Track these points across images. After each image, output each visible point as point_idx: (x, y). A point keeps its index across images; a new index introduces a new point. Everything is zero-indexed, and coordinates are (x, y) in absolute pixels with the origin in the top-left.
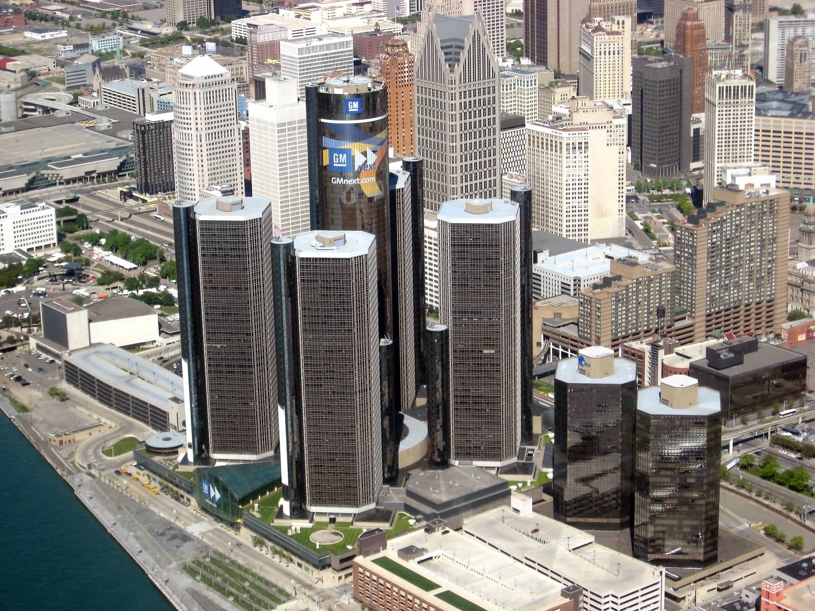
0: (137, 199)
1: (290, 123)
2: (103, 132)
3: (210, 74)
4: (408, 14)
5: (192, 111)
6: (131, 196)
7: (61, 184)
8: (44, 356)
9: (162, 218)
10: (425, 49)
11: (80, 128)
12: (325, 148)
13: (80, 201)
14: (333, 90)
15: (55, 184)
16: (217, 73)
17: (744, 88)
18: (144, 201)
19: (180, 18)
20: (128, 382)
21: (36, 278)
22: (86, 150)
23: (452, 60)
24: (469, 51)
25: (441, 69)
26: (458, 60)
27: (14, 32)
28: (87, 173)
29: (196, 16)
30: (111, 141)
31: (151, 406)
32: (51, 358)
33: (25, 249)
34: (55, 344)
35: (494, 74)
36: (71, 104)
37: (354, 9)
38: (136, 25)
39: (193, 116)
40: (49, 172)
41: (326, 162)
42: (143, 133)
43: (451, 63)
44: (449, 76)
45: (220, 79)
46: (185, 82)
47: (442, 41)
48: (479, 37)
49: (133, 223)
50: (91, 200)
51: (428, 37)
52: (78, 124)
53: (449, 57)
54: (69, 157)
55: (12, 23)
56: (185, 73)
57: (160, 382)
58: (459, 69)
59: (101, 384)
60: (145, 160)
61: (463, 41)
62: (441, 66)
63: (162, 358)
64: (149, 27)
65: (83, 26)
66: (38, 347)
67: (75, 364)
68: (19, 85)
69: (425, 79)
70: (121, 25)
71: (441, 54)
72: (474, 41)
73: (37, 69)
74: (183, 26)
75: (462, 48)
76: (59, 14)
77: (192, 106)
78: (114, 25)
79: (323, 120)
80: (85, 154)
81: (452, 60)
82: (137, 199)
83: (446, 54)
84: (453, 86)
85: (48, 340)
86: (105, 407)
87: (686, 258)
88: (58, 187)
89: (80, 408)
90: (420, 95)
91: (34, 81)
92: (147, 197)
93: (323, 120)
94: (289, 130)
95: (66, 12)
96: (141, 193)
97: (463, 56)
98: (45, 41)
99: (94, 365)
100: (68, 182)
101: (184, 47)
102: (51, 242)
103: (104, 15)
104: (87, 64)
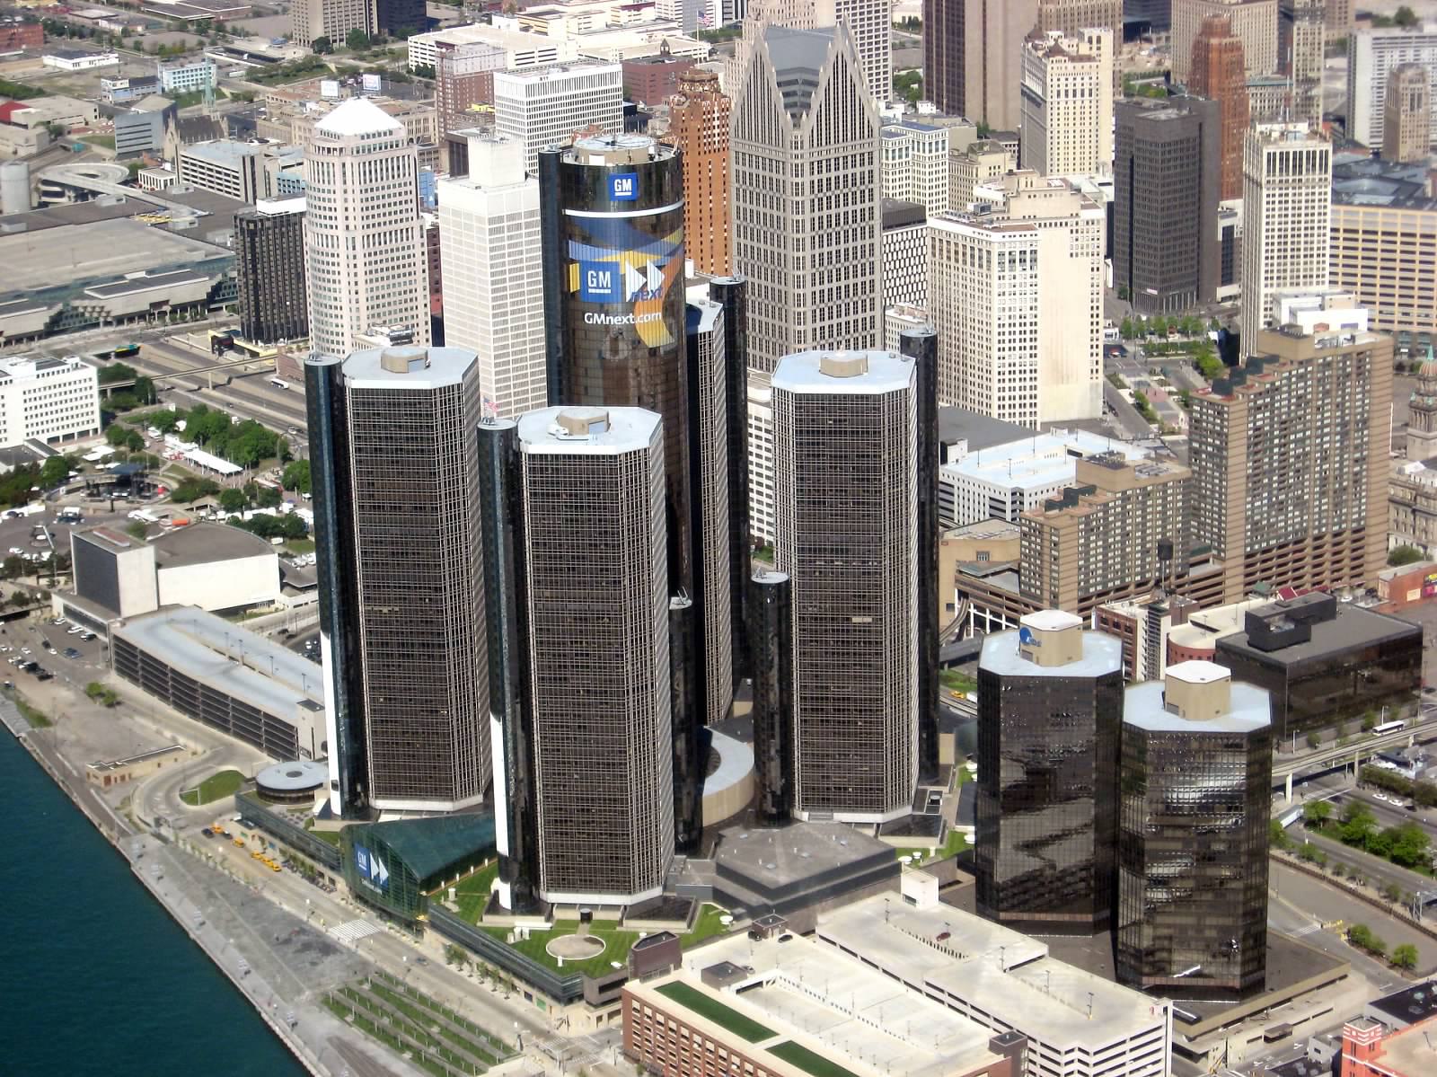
0: (241, 350)
1: (511, 217)
2: (182, 233)
3: (371, 131)
4: (719, 24)
5: (339, 196)
6: (231, 346)
7: (107, 324)
8: (77, 627)
9: (286, 385)
10: (749, 86)
11: (141, 226)
12: (573, 261)
13: (141, 354)
14: (587, 159)
15: (96, 325)
16: (382, 129)
17: (1311, 156)
18: (254, 355)
19: (318, 31)
20: (226, 673)
21: (63, 489)
22: (152, 264)
23: (798, 106)
24: (827, 90)
25: (777, 121)
26: (808, 106)
27: (25, 56)
28: (154, 305)
29: (346, 29)
30: (195, 249)
31: (267, 715)
32: (90, 632)
33: (43, 439)
34: (97, 606)
35: (871, 131)
36: (125, 183)
37: (624, 16)
38: (239, 44)
39: (339, 205)
40: (86, 303)
41: (575, 286)
42: (253, 234)
43: (795, 110)
44: (792, 134)
45: (388, 139)
46: (327, 145)
47: (779, 73)
48: (845, 66)
49: (234, 393)
50: (160, 352)
51: (755, 66)
52: (137, 218)
53: (791, 100)
54: (122, 277)
55: (22, 41)
56: (326, 128)
57: (282, 673)
58: (809, 121)
59: (179, 677)
60: (255, 282)
61: (816, 73)
62: (777, 116)
63: (285, 631)
64: (262, 47)
65: (146, 46)
66: (68, 611)
67: (132, 642)
68: (34, 150)
69: (750, 139)
70: (213, 43)
71: (778, 96)
72: (835, 73)
73: (66, 122)
74: (323, 45)
75: (815, 84)
76: (104, 24)
77: (339, 186)
78: (201, 44)
79: (569, 212)
80: (150, 272)
81: (798, 106)
82: (241, 350)
83: (786, 95)
84: (799, 152)
85: (84, 600)
86: (186, 718)
87: (1210, 455)
88: (103, 329)
89: (140, 720)
90: (741, 168)
91: (60, 142)
92: (259, 348)
93: (569, 212)
94: (510, 228)
95: (116, 22)
96: (249, 340)
97: (817, 99)
98: (80, 73)
99: (166, 644)
100: (120, 320)
101: (324, 83)
102: (90, 427)
103: (183, 27)
104: (153, 113)
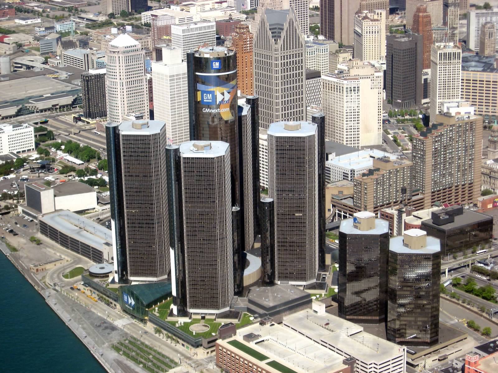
0: (83, 121)
1: (177, 75)
2: (63, 81)
3: (129, 45)
4: (249, 8)
5: (118, 68)
6: (80, 120)
7: (37, 112)
8: (27, 217)
9: (99, 133)
10: (259, 30)
11: (49, 78)
12: (199, 91)
13: (49, 123)
14: (203, 55)
15: (33, 113)
16: (133, 45)
17: (454, 54)
18: (88, 123)
19: (110, 11)
20: (78, 233)
21: (22, 169)
22: (53, 91)
23: (276, 37)
24: (287, 31)
25: (269, 42)
26: (280, 37)
27: (9, 20)
28: (53, 106)
29: (120, 10)
30: (68, 86)
31: (92, 248)
32: (31, 219)
33: (15, 152)
34: (33, 210)
35: (302, 45)
36: (43, 63)
37: (216, 6)
38: (83, 15)
39: (118, 71)
40: (30, 105)
41: (199, 99)
42: (88, 81)
43: (276, 38)
44: (274, 47)
45: (135, 48)
46: (113, 50)
47: (270, 25)
48: (293, 23)
49: (81, 136)
50: (55, 122)
51: (262, 23)
52: (47, 76)
53: (274, 35)
54: (42, 96)
55: (8, 14)
56: (113, 44)
57: (98, 233)
58: (280, 42)
59: (62, 235)
60: (89, 98)
61: (283, 25)
62: (269, 40)
63: (99, 219)
64: (91, 16)
65: (51, 16)
66: (24, 212)
67: (46, 222)
68: (12, 52)
69: (260, 48)
70: (74, 15)
71: (270, 33)
72: (290, 25)
73: (23, 42)
74: (112, 16)
75: (282, 29)
76: (36, 8)
77: (117, 64)
78: (70, 15)
79: (197, 73)
80: (52, 94)
81: (276, 37)
82: (83, 121)
83: (272, 33)
84: (277, 53)
85: (29, 208)
86: (64, 249)
87: (419, 157)
88: (36, 114)
89: (49, 249)
90: (257, 58)
91: (21, 49)
92: (90, 120)
93: (197, 73)
94: (177, 79)
95: (40, 8)
96: (86, 118)
97: (283, 34)
98: (28, 25)
100: (42, 111)
101: (112, 29)
102: (31, 148)
103: (63, 9)
104: (53, 39)
